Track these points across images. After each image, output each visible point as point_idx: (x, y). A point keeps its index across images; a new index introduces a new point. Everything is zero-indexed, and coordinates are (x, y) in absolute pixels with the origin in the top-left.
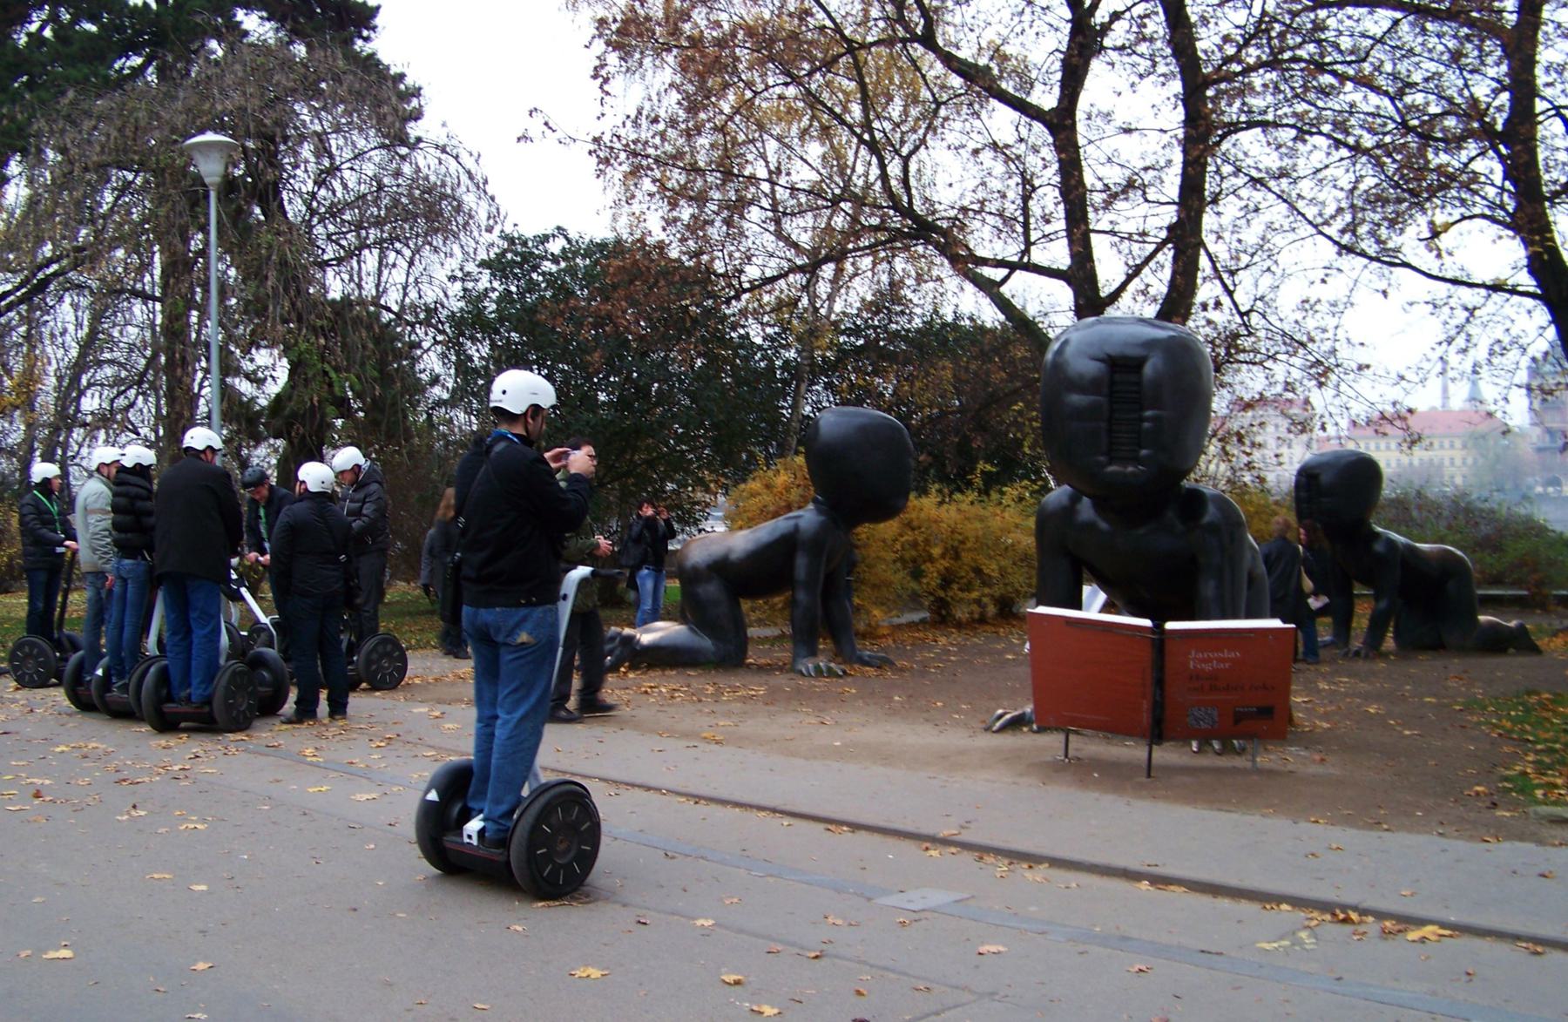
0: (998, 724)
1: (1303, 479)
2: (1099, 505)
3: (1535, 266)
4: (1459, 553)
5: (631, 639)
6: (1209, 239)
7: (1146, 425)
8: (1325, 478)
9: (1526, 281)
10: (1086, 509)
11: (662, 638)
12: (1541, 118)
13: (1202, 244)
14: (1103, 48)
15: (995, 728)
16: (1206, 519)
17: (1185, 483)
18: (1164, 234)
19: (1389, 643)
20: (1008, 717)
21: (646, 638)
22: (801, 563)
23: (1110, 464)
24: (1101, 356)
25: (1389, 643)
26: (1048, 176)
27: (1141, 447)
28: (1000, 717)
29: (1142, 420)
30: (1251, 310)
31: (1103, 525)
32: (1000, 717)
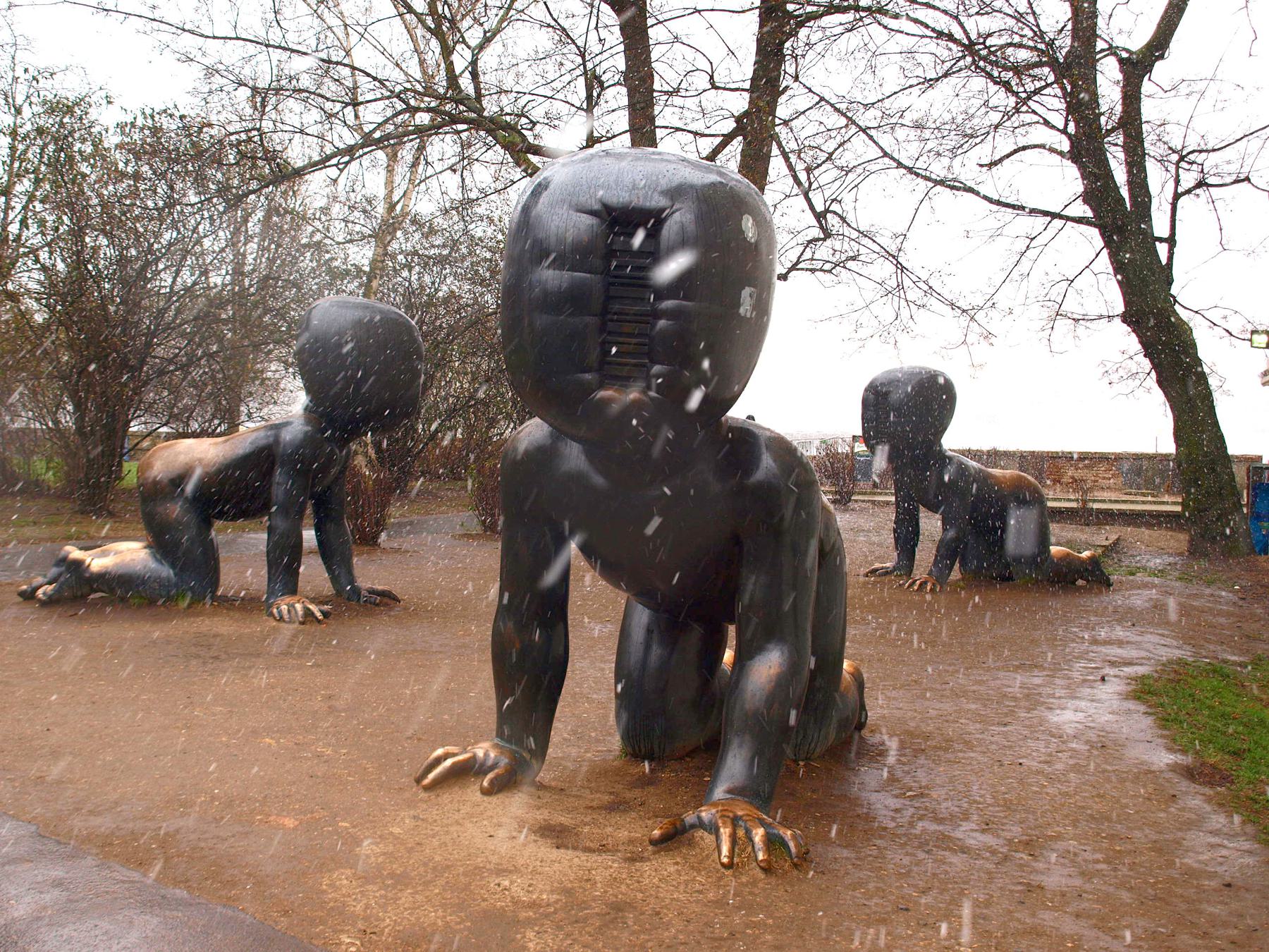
0: (431, 776)
1: (872, 396)
2: (593, 451)
3: (1087, 197)
4: (1030, 478)
5: (78, 565)
6: (781, 131)
7: (662, 323)
8: (896, 396)
9: (1081, 209)
10: (574, 456)
11: (116, 564)
12: (1098, 57)
13: (775, 138)
14: (757, 244)
15: (426, 782)
16: (759, 475)
17: (731, 413)
18: (730, 125)
19: (956, 574)
20: (449, 762)
21: (97, 562)
22: (281, 483)
23: (601, 386)
24: (597, 207)
25: (956, 574)
26: (614, 63)
27: (654, 362)
28: (438, 761)
29: (657, 315)
30: (827, 211)
31: (598, 480)
32: (438, 761)
